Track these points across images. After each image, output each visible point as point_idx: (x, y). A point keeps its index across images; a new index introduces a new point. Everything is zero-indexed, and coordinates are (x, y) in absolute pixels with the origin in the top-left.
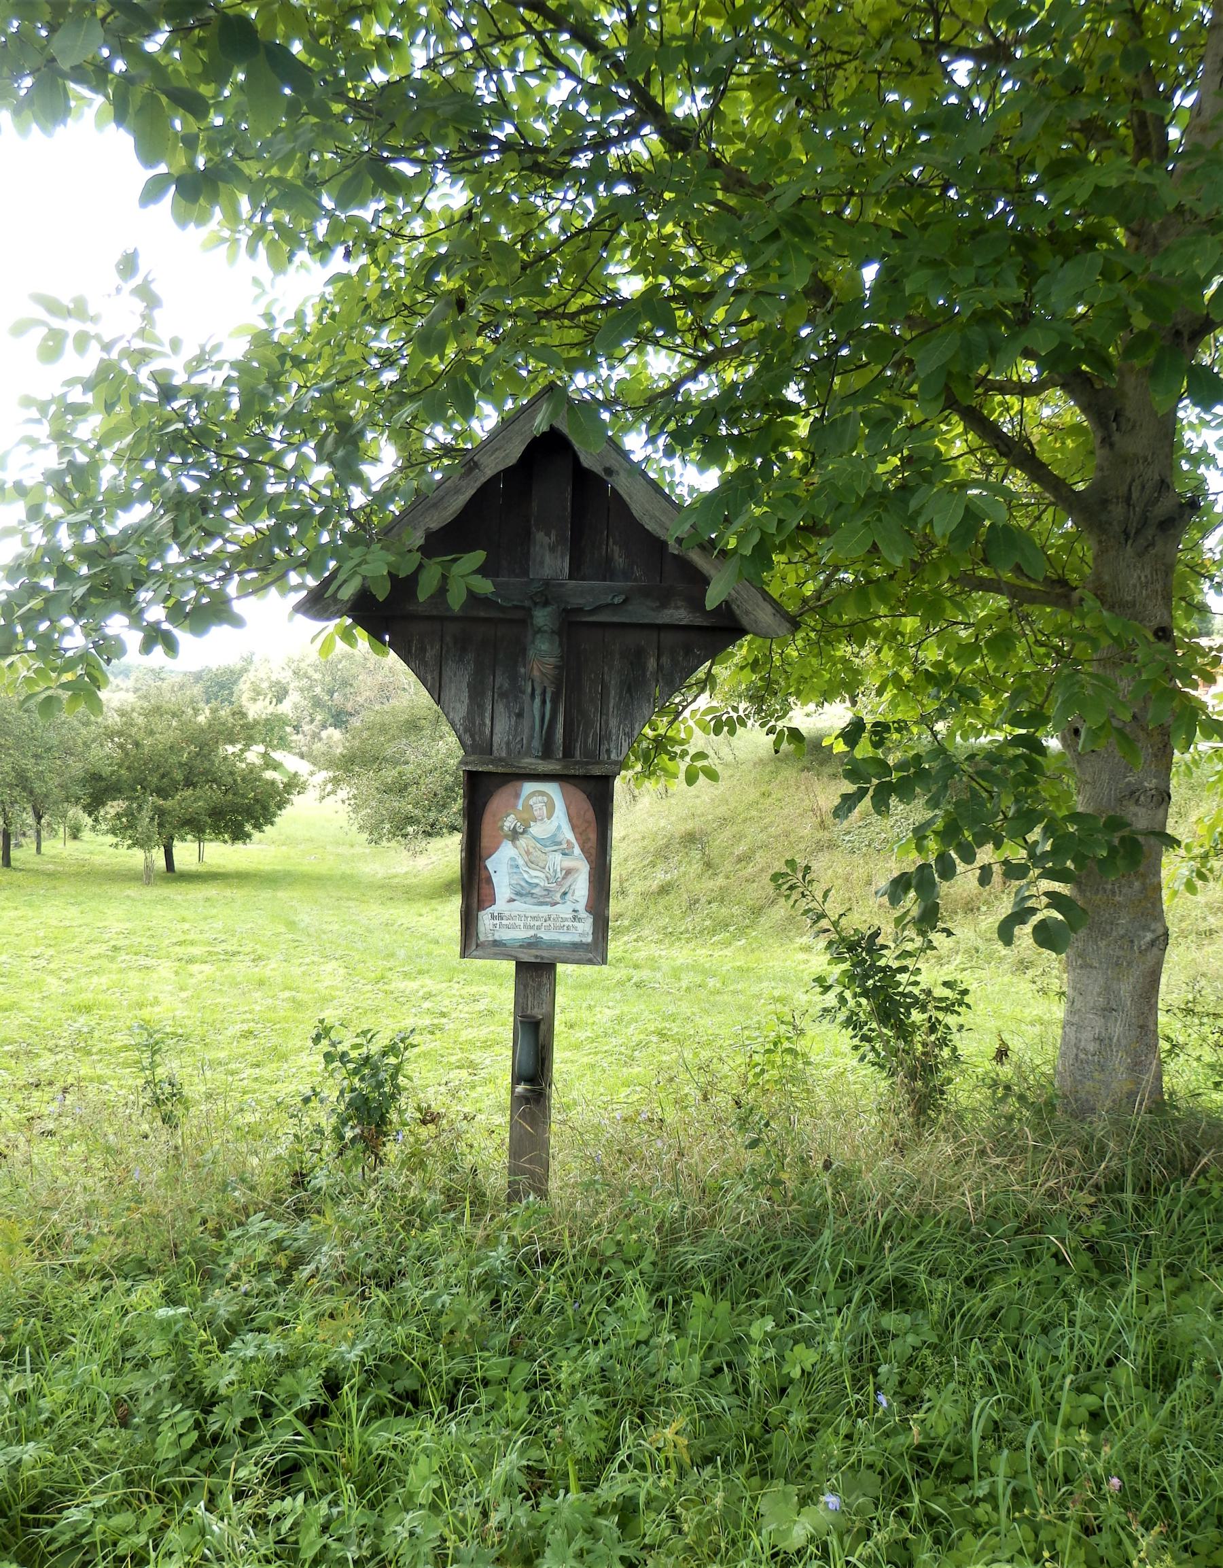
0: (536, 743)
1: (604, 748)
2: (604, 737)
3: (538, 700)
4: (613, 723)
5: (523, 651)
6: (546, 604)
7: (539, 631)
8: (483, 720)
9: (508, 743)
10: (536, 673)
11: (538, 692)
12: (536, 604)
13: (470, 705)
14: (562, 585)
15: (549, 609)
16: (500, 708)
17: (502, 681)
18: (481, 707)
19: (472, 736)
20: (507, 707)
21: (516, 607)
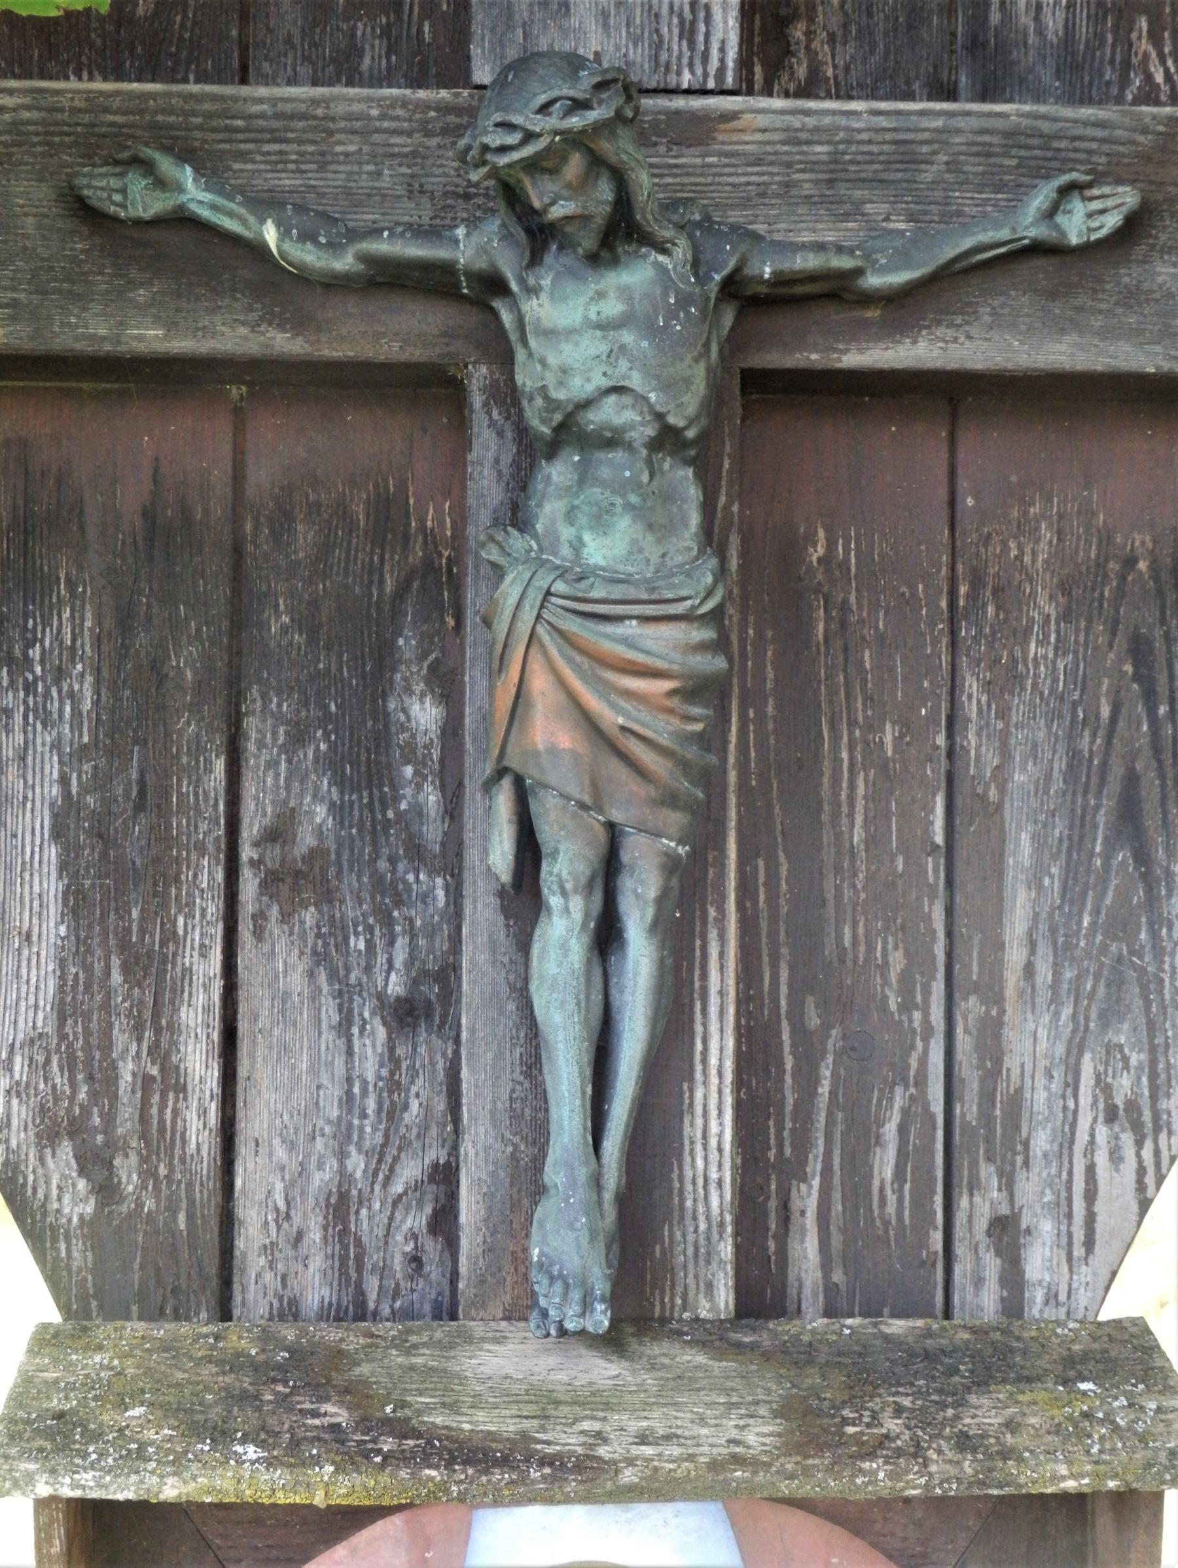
0: (568, 1239)
1: (978, 1208)
2: (972, 1138)
3: (563, 930)
4: (1032, 1041)
5: (441, 586)
6: (621, 233)
7: (570, 432)
8: (163, 1054)
9: (340, 1207)
10: (549, 734)
11: (567, 863)
12: (539, 236)
13: (77, 949)
14: (696, 131)
15: (637, 275)
16: (280, 965)
17: (287, 788)
18: (153, 969)
19: (95, 1164)
20: (326, 957)
21: (389, 279)
